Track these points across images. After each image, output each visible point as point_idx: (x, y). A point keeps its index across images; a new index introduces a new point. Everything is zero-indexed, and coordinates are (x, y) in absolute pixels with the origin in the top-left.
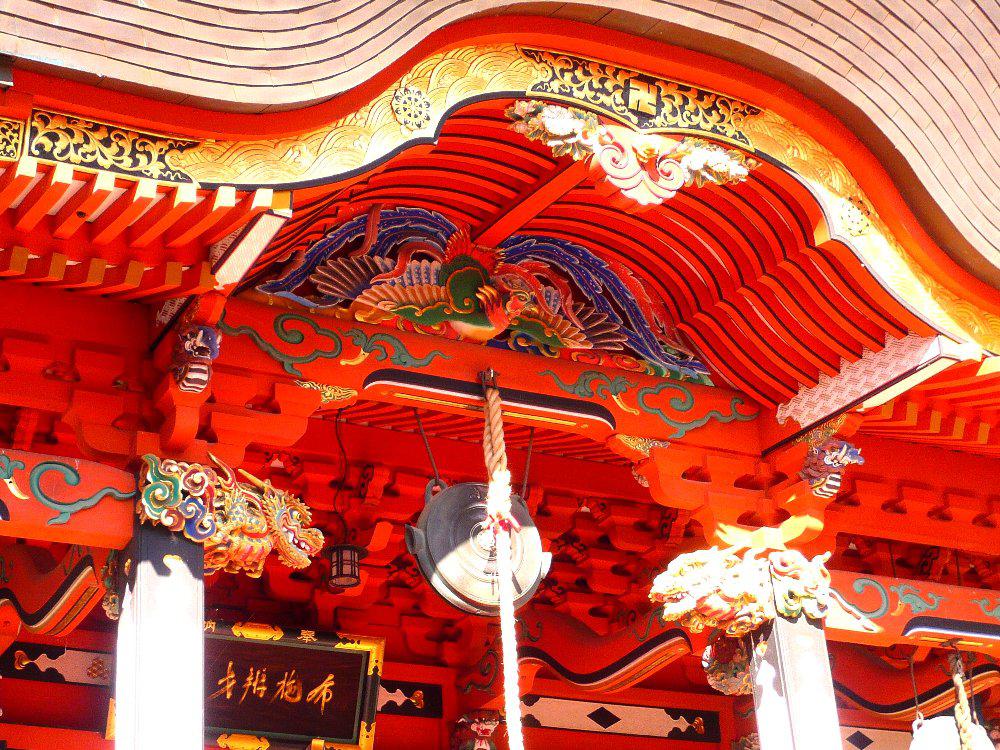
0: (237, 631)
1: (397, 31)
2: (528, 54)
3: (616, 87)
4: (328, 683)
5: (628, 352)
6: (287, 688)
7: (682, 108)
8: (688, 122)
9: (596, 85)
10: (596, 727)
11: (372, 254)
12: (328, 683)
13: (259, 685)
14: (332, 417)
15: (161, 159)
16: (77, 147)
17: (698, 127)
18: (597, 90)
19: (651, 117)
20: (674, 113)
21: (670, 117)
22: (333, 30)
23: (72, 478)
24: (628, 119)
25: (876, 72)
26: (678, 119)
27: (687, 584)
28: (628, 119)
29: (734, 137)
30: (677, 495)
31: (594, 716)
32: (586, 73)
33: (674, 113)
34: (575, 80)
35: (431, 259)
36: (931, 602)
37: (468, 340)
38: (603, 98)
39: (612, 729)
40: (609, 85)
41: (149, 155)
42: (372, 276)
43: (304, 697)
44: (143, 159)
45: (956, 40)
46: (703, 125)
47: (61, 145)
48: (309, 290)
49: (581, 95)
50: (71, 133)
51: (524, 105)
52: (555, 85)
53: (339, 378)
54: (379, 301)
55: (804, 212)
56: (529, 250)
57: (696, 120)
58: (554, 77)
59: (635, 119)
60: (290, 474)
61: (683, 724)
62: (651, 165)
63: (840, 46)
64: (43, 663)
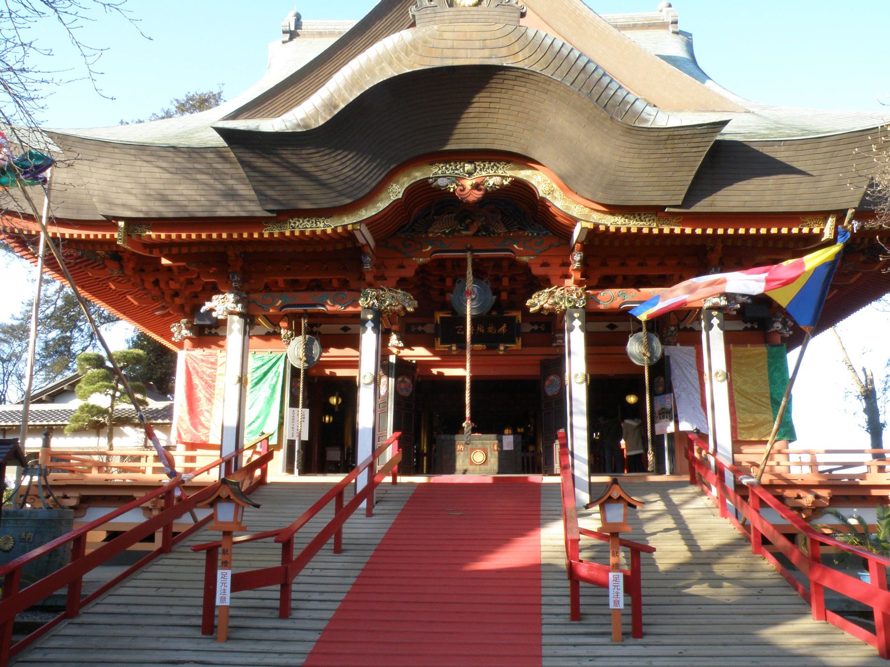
4: (504, 326)
6: (491, 329)
10: (343, 332)
12: (504, 326)
20: (481, 170)
27: (539, 301)
30: (537, 271)
31: (608, 327)
33: (481, 170)
39: (616, 330)
53: (423, 255)
60: (402, 284)
64: (536, 327)
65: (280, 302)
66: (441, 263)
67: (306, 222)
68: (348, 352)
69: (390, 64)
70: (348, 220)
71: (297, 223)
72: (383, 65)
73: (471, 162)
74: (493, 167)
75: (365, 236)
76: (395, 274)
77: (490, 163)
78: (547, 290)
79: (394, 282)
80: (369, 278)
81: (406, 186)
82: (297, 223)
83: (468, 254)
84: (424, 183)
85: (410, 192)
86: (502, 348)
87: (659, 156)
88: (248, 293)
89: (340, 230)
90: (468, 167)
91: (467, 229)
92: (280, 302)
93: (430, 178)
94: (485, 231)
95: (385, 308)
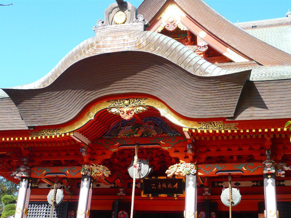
0: (159, 178)
1: (78, 108)
2: (108, 102)
3: (122, 102)
4: (177, 184)
5: (163, 133)
6: (169, 186)
7: (134, 102)
8: (135, 104)
9: (119, 103)
11: (121, 127)
12: (177, 184)
13: (165, 186)
14: (115, 153)
15: (56, 132)
16: (46, 133)
17: (136, 104)
18: (119, 104)
19: (128, 105)
21: (131, 104)
22: (68, 111)
23: (75, 169)
24: (124, 106)
25: (156, 90)
26: (133, 104)
27: (172, 171)
28: (124, 106)
29: (143, 104)
30: (173, 155)
31: (239, 184)
32: (117, 102)
34: (115, 103)
35: (130, 125)
36: (222, 167)
37: (136, 137)
38: (120, 105)
40: (121, 102)
41: (55, 132)
42: (120, 130)
43: (173, 187)
44: (54, 132)
45: (165, 82)
46: (137, 104)
47: (44, 133)
48: (111, 135)
49: (116, 105)
50: (45, 131)
51: (108, 109)
52: (112, 105)
53: (115, 147)
54: (121, 135)
55: (157, 113)
56: (148, 120)
57: (136, 103)
58: (112, 104)
59: (126, 106)
60: (105, 163)
61: (255, 184)
62: (128, 113)
63: (148, 88)
65: (215, 169)
66: (122, 152)
67: (48, 132)
68: (30, 200)
69: (81, 54)
70: (67, 131)
71: (45, 132)
72: (78, 55)
73: (127, 100)
74: (138, 101)
75: (80, 138)
76: (100, 158)
77: (137, 99)
78: (177, 165)
79: (99, 162)
80: (85, 160)
81: (96, 113)
82: (45, 132)
83: (135, 147)
84: (105, 111)
85: (98, 116)
86: (175, 196)
87: (217, 91)
88: (31, 167)
89: (63, 135)
90: (126, 102)
91: (136, 133)
92: (215, 169)
93: (107, 108)
94: (146, 134)
95: (94, 175)
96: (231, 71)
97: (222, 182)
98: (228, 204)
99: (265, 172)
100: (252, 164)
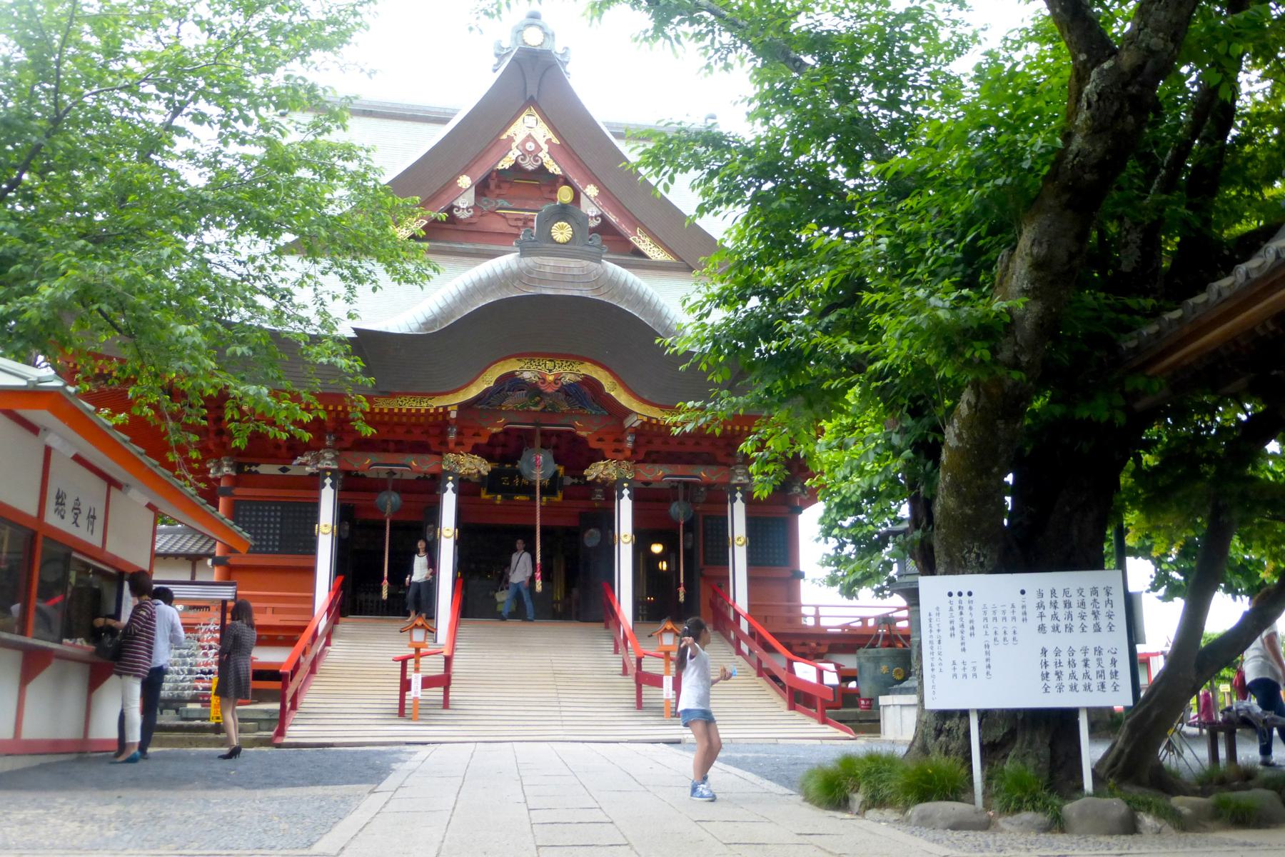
14: (495, 435)
60: (476, 450)
61: (254, 468)
80: (452, 446)
85: (501, 380)
96: (578, 265)
97: (257, 465)
98: (530, 549)
99: (734, 482)
100: (715, 468)
